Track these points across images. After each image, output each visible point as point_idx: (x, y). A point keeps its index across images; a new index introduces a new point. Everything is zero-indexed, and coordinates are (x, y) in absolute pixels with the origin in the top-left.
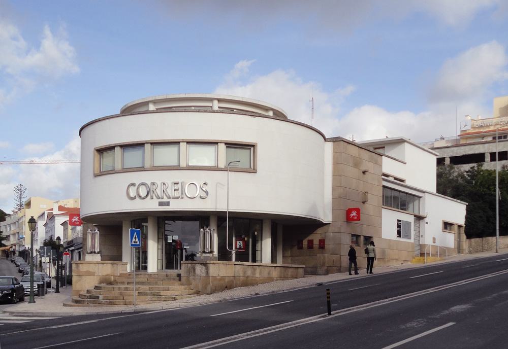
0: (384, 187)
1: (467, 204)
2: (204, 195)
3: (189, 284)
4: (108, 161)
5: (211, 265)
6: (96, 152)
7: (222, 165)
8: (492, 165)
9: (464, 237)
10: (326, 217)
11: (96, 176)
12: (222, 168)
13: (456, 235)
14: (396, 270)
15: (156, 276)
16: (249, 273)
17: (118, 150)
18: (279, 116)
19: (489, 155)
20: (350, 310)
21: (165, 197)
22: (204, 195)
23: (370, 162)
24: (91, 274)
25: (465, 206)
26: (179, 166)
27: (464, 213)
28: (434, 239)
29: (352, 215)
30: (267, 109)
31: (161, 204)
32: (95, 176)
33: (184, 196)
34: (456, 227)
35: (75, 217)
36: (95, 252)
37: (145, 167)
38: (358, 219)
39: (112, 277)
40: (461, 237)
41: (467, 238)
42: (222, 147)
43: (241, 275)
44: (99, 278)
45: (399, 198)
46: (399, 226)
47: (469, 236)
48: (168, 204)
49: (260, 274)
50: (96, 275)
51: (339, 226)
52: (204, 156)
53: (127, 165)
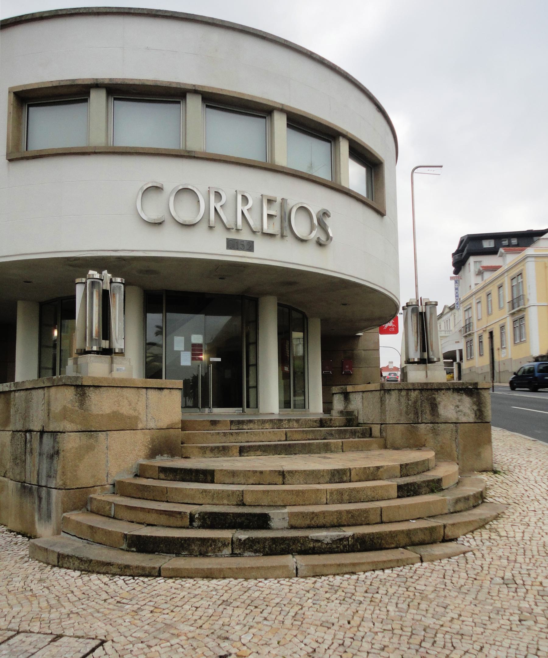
4: (50, 126)
17: (98, 98)
24: (128, 424)
31: (232, 244)
32: (10, 160)
33: (287, 232)
44: (148, 438)
48: (250, 246)
50: (140, 426)
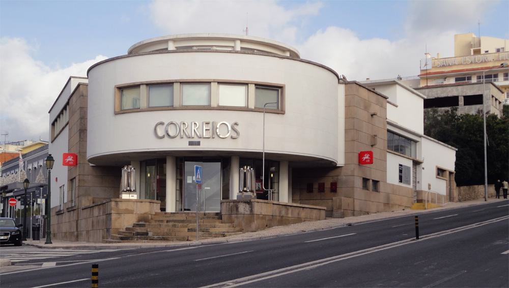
0: (389, 131)
1: (457, 150)
2: (235, 135)
3: (232, 222)
5: (256, 204)
6: (116, 89)
7: (252, 106)
8: (467, 108)
9: (454, 184)
10: (340, 161)
11: (116, 114)
12: (252, 109)
13: (448, 182)
14: (405, 214)
15: (194, 215)
16: (283, 213)
17: (143, 88)
18: (294, 56)
19: (463, 98)
20: (428, 237)
21: (195, 136)
22: (235, 135)
23: (377, 104)
24: (131, 212)
25: (455, 152)
26: (173, 106)
27: (454, 159)
28: (429, 185)
29: (364, 158)
30: (284, 50)
31: (191, 143)
32: (116, 114)
33: (215, 136)
34: (448, 173)
35: (69, 157)
36: (130, 191)
37: (174, 106)
38: (371, 162)
39: (150, 216)
40: (452, 185)
41: (457, 186)
42: (252, 88)
43: (277, 214)
44: (137, 216)
45: (400, 142)
46: (401, 171)
47: (459, 185)
48: (198, 143)
49: (292, 215)
50: (134, 213)
51: (352, 169)
52: (235, 96)
53: (153, 104)
